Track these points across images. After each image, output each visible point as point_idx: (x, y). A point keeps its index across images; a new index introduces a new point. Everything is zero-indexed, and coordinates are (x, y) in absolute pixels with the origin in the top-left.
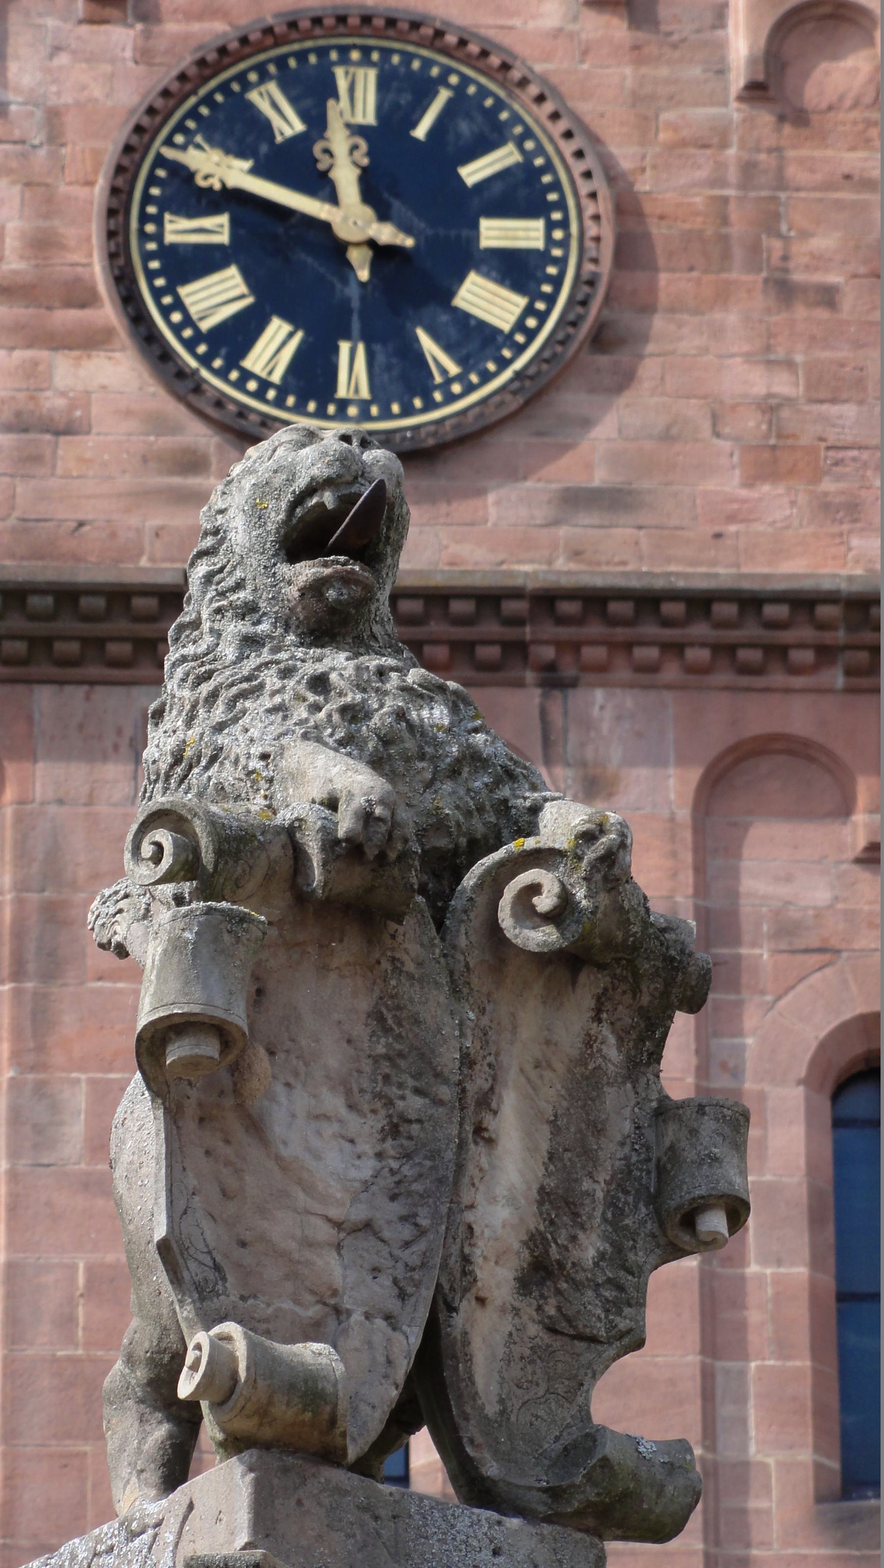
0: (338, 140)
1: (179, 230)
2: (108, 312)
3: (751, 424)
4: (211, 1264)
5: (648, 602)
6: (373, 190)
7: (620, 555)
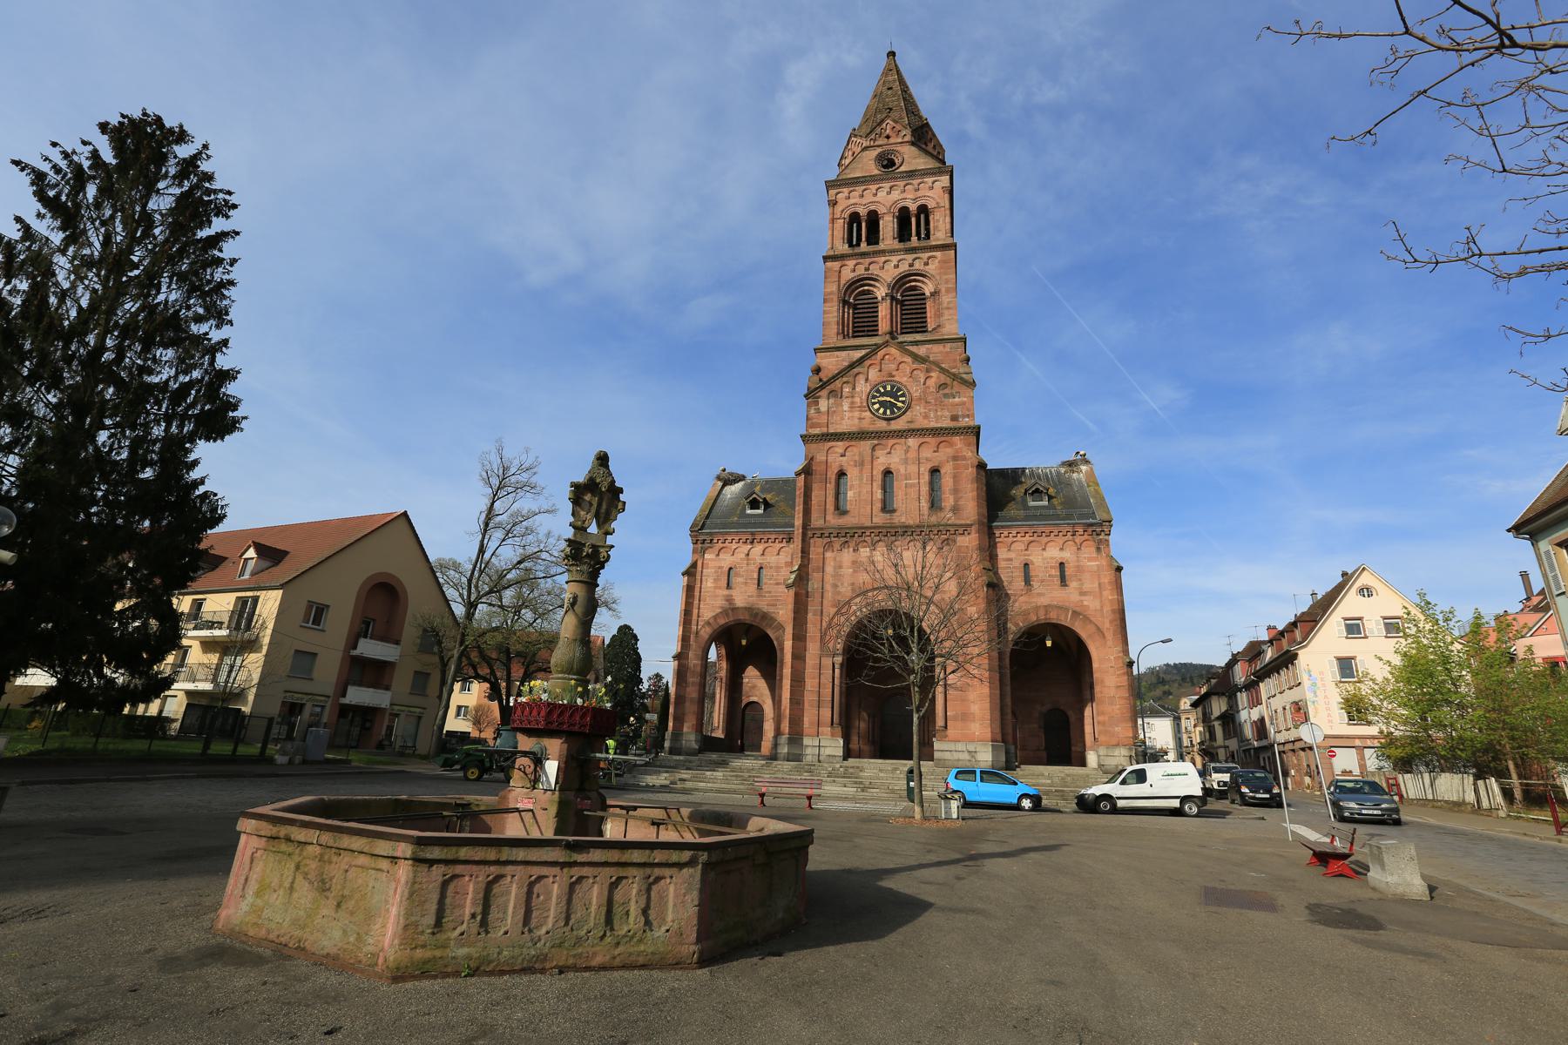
7: (912, 426)
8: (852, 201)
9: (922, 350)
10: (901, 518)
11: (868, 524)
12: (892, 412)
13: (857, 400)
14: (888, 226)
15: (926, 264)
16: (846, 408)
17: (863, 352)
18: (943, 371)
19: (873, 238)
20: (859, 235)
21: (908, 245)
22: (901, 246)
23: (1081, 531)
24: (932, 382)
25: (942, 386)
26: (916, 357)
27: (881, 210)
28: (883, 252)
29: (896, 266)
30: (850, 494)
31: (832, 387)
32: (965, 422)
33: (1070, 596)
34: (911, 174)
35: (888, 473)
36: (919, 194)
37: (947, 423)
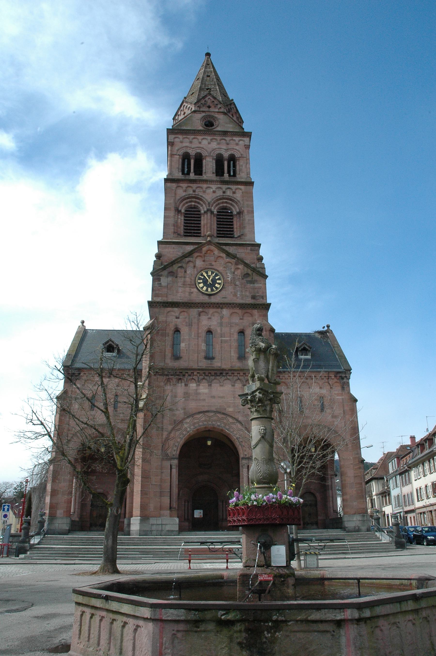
0: (212, 276)
1: (199, 281)
2: (194, 286)
3: (233, 293)
4: (40, 423)
5: (227, 304)
6: (212, 280)
7: (226, 301)
8: (184, 145)
9: (232, 250)
10: (217, 364)
11: (195, 366)
12: (212, 290)
13: (188, 279)
14: (209, 165)
15: (234, 193)
16: (180, 284)
17: (190, 248)
18: (246, 265)
19: (199, 170)
20: (189, 168)
21: (222, 178)
22: (218, 178)
23: (333, 376)
24: (238, 272)
25: (246, 275)
26: (228, 254)
27: (204, 154)
28: (206, 181)
29: (214, 192)
30: (183, 345)
31: (170, 269)
32: (261, 301)
33: (327, 416)
34: (225, 133)
35: (209, 332)
36: (230, 147)
37: (249, 301)
